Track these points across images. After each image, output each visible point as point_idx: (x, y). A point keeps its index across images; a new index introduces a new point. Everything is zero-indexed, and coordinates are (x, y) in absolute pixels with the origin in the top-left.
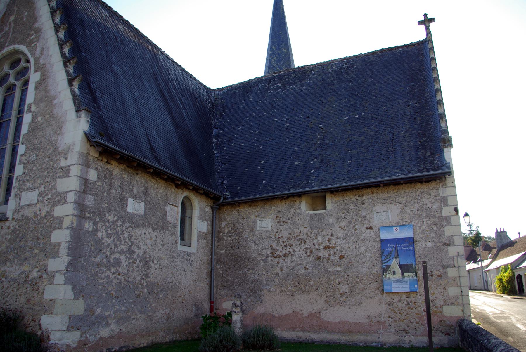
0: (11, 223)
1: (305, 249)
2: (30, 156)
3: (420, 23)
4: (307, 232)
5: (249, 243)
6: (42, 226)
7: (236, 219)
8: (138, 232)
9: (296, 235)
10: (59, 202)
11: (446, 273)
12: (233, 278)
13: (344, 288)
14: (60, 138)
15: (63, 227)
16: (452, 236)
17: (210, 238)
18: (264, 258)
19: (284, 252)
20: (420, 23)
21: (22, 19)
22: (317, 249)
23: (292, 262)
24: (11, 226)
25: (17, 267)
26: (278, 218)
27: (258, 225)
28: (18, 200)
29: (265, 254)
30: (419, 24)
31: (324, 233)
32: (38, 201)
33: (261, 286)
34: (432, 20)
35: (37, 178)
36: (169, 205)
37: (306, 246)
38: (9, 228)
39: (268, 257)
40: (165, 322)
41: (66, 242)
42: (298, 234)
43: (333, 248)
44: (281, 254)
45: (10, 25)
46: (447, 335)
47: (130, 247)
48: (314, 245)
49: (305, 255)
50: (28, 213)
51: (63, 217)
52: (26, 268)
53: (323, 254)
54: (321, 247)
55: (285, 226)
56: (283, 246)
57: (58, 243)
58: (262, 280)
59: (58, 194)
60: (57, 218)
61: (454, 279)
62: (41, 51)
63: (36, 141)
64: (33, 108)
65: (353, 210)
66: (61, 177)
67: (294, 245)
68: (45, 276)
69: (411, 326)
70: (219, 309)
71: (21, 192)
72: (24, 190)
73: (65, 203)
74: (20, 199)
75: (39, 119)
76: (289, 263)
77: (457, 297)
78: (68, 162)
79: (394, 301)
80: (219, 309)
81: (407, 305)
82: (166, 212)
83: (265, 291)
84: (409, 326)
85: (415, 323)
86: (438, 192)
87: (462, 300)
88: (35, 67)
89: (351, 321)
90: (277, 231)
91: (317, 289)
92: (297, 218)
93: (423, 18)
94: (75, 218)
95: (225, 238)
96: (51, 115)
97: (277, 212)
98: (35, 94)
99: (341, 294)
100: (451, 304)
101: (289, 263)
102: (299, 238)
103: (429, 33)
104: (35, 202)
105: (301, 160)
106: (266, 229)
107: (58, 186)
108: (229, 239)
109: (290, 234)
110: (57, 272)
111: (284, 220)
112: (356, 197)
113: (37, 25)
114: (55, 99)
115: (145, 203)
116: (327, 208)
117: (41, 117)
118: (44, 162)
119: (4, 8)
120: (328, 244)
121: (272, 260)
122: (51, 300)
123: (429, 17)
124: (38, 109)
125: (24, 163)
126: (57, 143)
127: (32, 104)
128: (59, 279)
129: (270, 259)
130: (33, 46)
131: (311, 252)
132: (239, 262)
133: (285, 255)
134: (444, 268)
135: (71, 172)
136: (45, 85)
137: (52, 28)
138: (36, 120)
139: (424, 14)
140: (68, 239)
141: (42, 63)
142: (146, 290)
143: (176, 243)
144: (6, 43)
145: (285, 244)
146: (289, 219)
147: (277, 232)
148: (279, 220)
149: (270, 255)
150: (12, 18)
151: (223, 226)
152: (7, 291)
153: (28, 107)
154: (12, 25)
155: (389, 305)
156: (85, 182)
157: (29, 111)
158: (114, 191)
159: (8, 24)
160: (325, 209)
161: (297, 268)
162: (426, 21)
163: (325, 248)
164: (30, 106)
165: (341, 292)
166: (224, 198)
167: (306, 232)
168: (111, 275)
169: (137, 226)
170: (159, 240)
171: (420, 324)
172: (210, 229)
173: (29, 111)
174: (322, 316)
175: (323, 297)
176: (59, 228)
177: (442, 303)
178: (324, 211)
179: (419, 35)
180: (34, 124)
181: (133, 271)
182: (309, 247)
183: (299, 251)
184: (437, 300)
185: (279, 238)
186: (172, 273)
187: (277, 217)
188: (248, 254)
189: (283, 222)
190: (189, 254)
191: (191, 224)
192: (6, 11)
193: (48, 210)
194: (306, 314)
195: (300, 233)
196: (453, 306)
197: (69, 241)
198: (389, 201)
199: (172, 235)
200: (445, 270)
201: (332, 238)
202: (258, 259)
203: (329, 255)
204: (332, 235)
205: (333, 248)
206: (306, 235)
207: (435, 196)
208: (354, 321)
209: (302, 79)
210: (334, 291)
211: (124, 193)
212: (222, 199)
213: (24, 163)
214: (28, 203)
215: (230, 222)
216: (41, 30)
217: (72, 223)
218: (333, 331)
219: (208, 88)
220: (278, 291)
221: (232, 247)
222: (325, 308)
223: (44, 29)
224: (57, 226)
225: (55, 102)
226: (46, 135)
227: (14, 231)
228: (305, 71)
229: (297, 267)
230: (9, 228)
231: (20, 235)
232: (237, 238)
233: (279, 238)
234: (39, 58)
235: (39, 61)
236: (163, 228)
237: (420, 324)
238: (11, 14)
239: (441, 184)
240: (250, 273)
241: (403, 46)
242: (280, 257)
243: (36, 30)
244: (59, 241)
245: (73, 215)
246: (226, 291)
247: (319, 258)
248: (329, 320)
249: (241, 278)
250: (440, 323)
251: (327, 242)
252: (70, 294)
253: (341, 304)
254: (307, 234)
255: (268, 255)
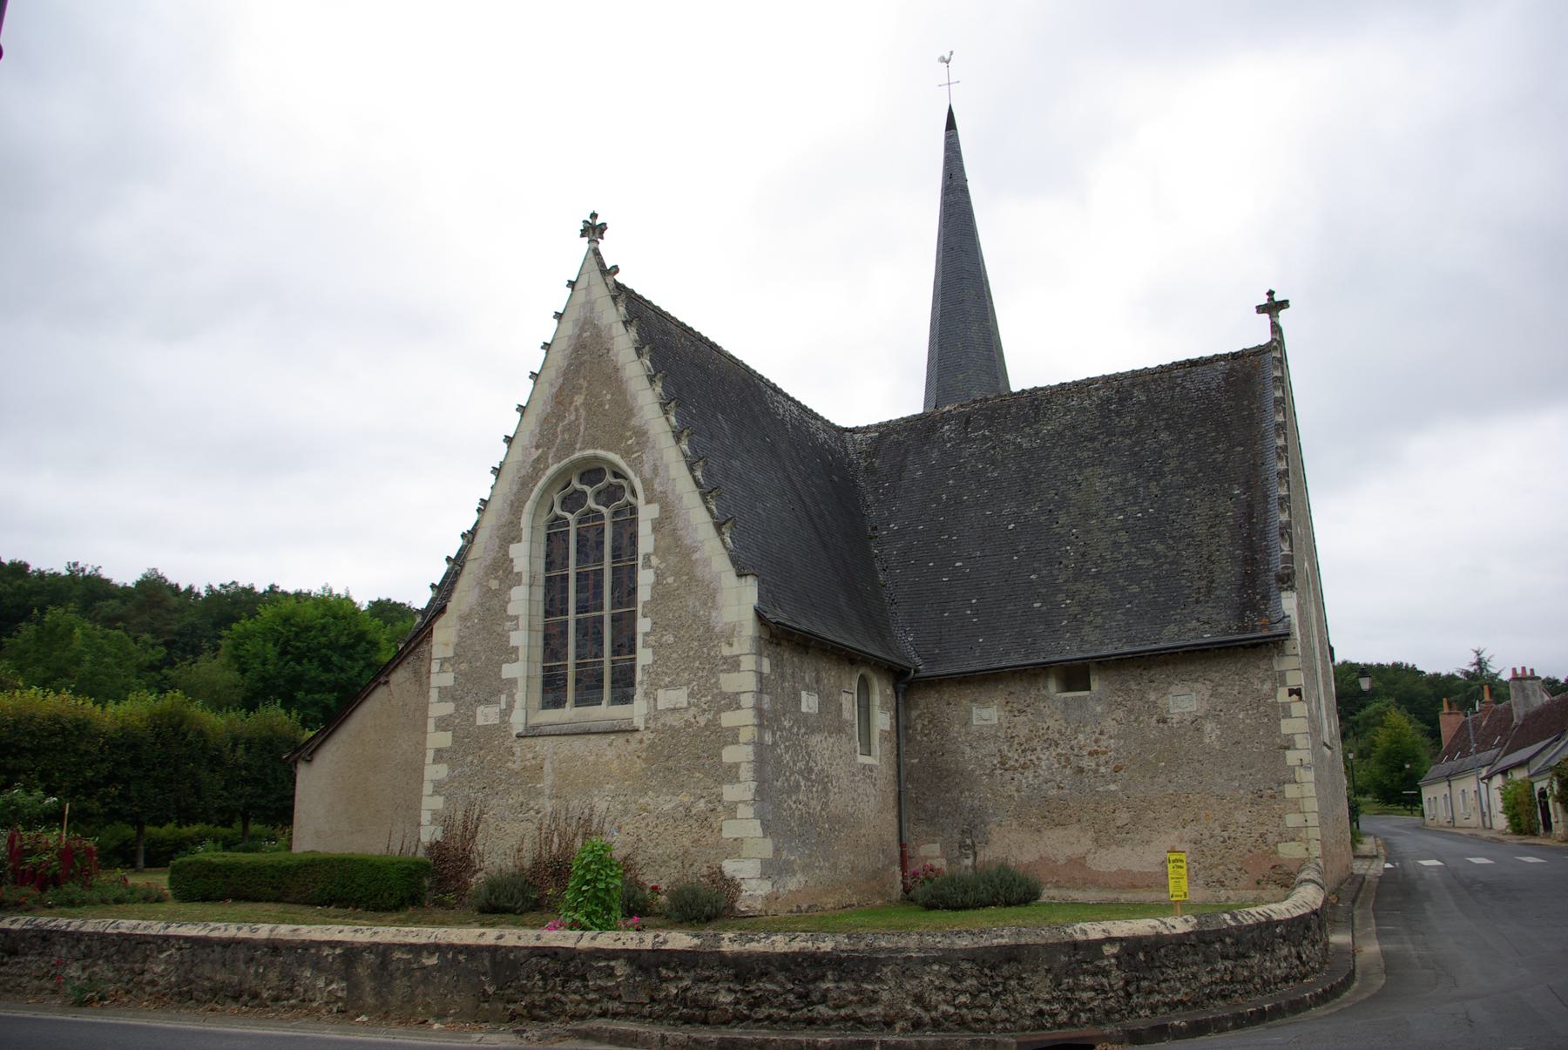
0: (644, 735)
1: (1057, 755)
2: (662, 636)
3: (1261, 309)
4: (1060, 727)
5: (961, 746)
6: (703, 739)
7: (935, 705)
8: (815, 740)
9: (1042, 732)
10: (729, 707)
11: (1282, 792)
12: (935, 806)
13: (1123, 817)
14: (714, 614)
15: (741, 741)
16: (1293, 734)
17: (895, 739)
18: (988, 772)
19: (1022, 761)
20: (1261, 309)
21: (601, 405)
22: (1077, 756)
23: (1035, 777)
24: (644, 738)
25: (668, 798)
26: (1010, 704)
27: (974, 716)
28: (652, 701)
29: (989, 765)
30: (1258, 312)
31: (1088, 729)
32: (689, 703)
33: (986, 817)
34: (1284, 304)
35: (682, 670)
36: (843, 694)
37: (1059, 750)
38: (641, 742)
39: (995, 769)
40: (849, 873)
41: (748, 762)
42: (1044, 731)
43: (1104, 753)
44: (1017, 765)
45: (577, 410)
46: (1283, 888)
47: (808, 762)
48: (1072, 748)
49: (1057, 766)
50: (674, 721)
51: (738, 728)
52: (685, 798)
53: (1089, 763)
54: (1085, 753)
55: (1023, 718)
56: (1020, 751)
57: (735, 763)
58: (986, 808)
59: (723, 695)
60: (728, 729)
61: (1296, 802)
62: (654, 469)
63: (671, 615)
64: (655, 561)
65: (1136, 692)
66: (728, 671)
67: (1039, 749)
68: (720, 808)
69: (1229, 874)
70: (913, 857)
71: (656, 690)
72: (661, 687)
73: (738, 708)
74: (655, 700)
75: (670, 580)
76: (1030, 779)
77: (1298, 829)
78: (735, 650)
79: (1203, 837)
80: (913, 857)
81: (1223, 842)
82: (841, 705)
83: (992, 826)
84: (1225, 875)
85: (1234, 870)
86: (1272, 663)
87: (1307, 833)
88: (646, 495)
89: (1135, 869)
90: (1008, 725)
91: (1080, 821)
92: (1042, 705)
93: (1264, 300)
94: (756, 729)
95: (919, 738)
96: (692, 577)
97: (1007, 693)
98: (655, 540)
99: (1118, 828)
100: (1290, 841)
101: (1030, 779)
102: (1046, 737)
103: (1276, 329)
104: (685, 704)
105: (1044, 599)
106: (989, 723)
107: (722, 685)
108: (925, 739)
109: (1032, 731)
110: (740, 802)
111: (1020, 707)
112: (1139, 670)
113: (634, 422)
114: (694, 552)
115: (819, 695)
116: (1092, 688)
117: (672, 578)
118: (692, 648)
119: (557, 378)
120: (1096, 748)
121: (1001, 774)
122: (735, 840)
123: (1277, 298)
124: (664, 565)
125: (653, 647)
126: (711, 621)
127: (651, 554)
128: (745, 811)
129: (998, 772)
130: (636, 458)
131: (1068, 760)
132: (945, 778)
133: (1024, 767)
134: (1279, 784)
135: (742, 665)
136: (672, 527)
137: (666, 432)
138: (665, 582)
139: (1268, 291)
140: (752, 758)
141: (659, 490)
142: (827, 826)
143: (855, 752)
144: (576, 443)
145: (1023, 747)
146: (1029, 706)
147: (1009, 728)
148: (1012, 707)
149: (998, 765)
150: (579, 400)
151: (913, 717)
152: (656, 830)
153: (644, 559)
154: (582, 412)
155: (1195, 843)
156: (760, 675)
157: (647, 564)
158: (787, 684)
159: (572, 408)
160: (1089, 689)
161: (1044, 787)
162: (1273, 307)
163: (1090, 754)
164: (647, 557)
165: (1119, 824)
166: (916, 671)
167: (1057, 727)
168: (791, 803)
169: (813, 732)
170: (836, 749)
171: (1243, 871)
172: (895, 724)
173: (647, 564)
174: (1089, 863)
175: (1090, 833)
176: (733, 743)
177: (1277, 839)
178: (1086, 693)
179: (1257, 333)
180: (660, 587)
181: (813, 799)
182: (1064, 752)
183: (1048, 759)
184: (1269, 834)
185: (1013, 737)
186: (853, 798)
187: (1007, 703)
188: (960, 765)
189: (1019, 711)
190: (871, 768)
191: (869, 719)
192: (564, 384)
193: (710, 717)
194: (1062, 862)
195: (1048, 728)
196: (1293, 843)
197: (753, 761)
198: (1193, 677)
199: (849, 740)
200: (1281, 788)
201: (1102, 737)
202: (977, 773)
203: (1098, 765)
204: (1101, 733)
205: (1104, 753)
206: (1058, 732)
207: (1267, 670)
208: (1141, 869)
209: (1033, 420)
210: (1107, 822)
211: (796, 685)
212: (913, 672)
213: (653, 647)
214: (672, 707)
215: (925, 711)
216: (646, 433)
217: (754, 737)
218: (1107, 886)
219: (838, 427)
220: (1015, 824)
221: (931, 754)
222: (1093, 851)
223: (651, 433)
224: (730, 739)
225: (695, 556)
226: (687, 606)
227: (652, 746)
228: (1040, 399)
229: (1045, 785)
230: (641, 742)
231: (666, 753)
232: (939, 737)
233: (1013, 737)
234: (652, 480)
235: (653, 486)
236: (840, 730)
237: (1243, 871)
238: (576, 390)
239: (1276, 651)
240: (965, 797)
241: (1228, 355)
242: (1015, 769)
243: (636, 430)
244: (738, 761)
245: (753, 725)
246: (925, 828)
247: (1081, 770)
248: (1101, 870)
249: (950, 805)
250: (1273, 870)
251: (1094, 744)
252: (759, 832)
253: (1119, 844)
254: (1059, 732)
255: (995, 765)
